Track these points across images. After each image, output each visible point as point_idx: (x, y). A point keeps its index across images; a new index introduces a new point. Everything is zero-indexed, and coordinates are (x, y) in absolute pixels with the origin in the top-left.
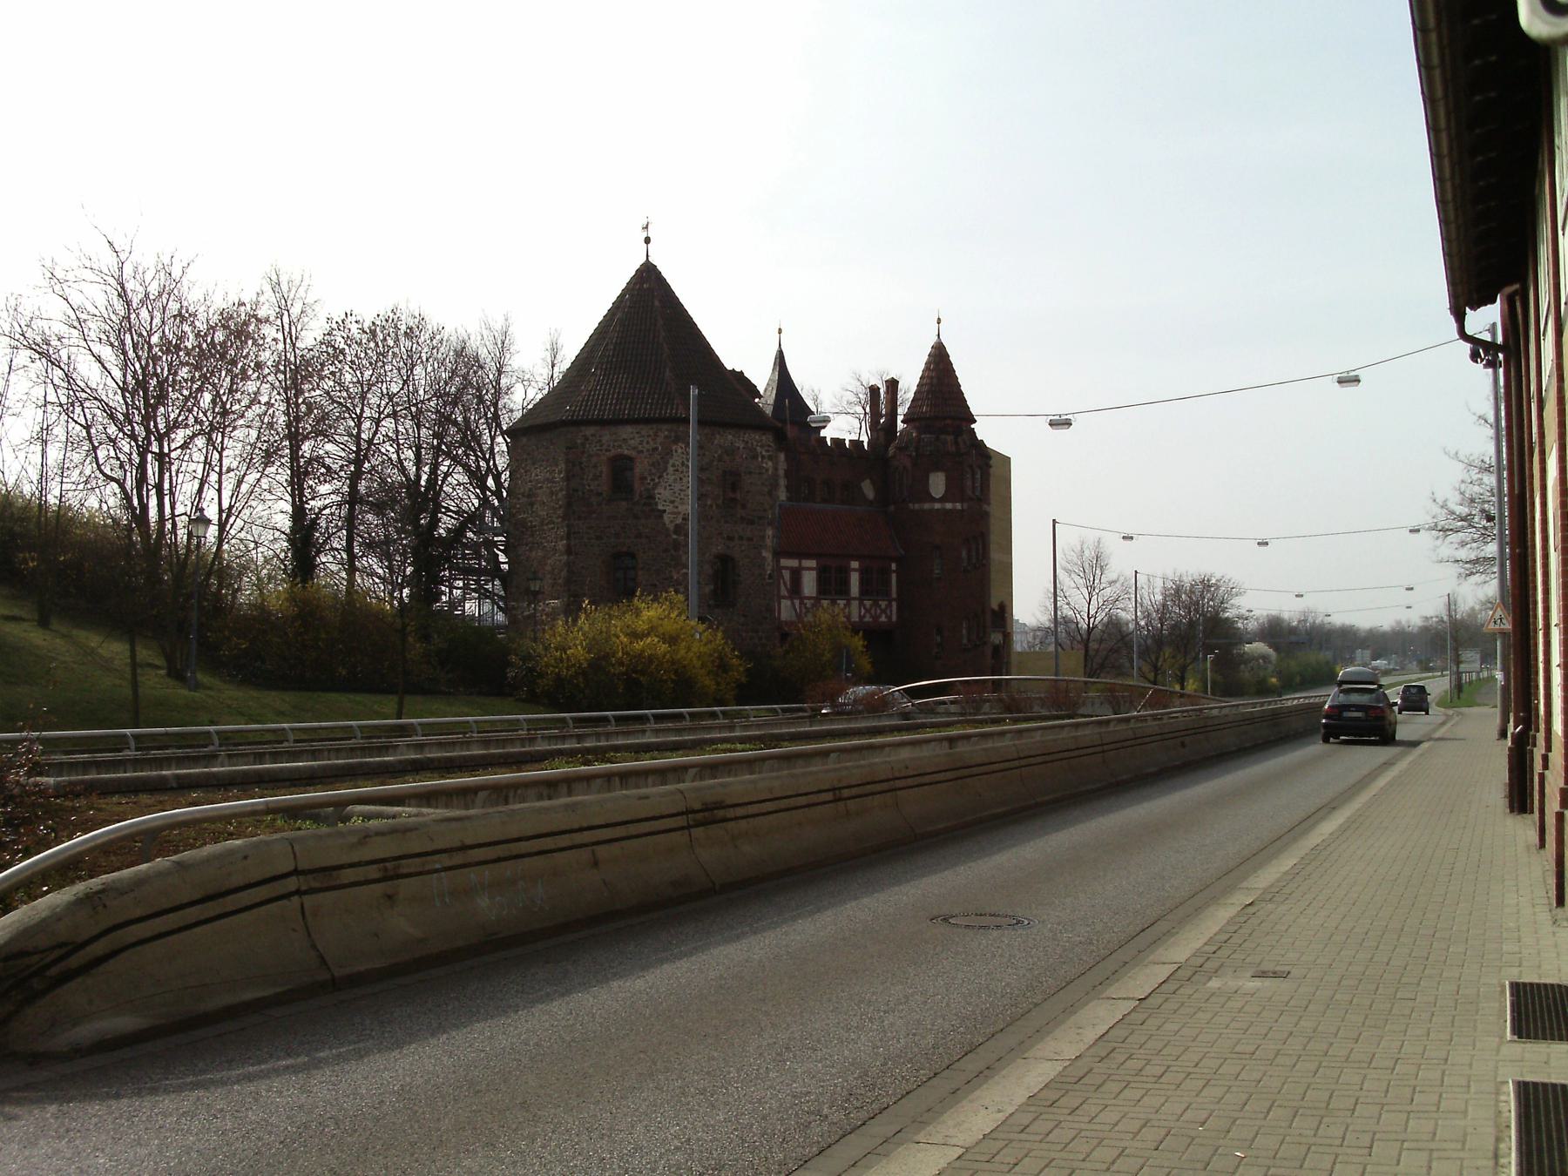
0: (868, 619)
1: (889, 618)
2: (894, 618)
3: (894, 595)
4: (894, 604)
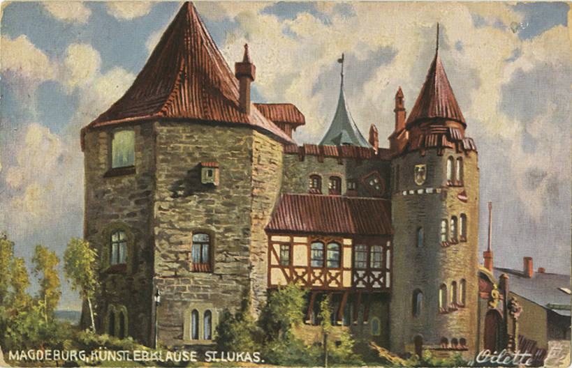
0: (360, 285)
1: (340, 284)
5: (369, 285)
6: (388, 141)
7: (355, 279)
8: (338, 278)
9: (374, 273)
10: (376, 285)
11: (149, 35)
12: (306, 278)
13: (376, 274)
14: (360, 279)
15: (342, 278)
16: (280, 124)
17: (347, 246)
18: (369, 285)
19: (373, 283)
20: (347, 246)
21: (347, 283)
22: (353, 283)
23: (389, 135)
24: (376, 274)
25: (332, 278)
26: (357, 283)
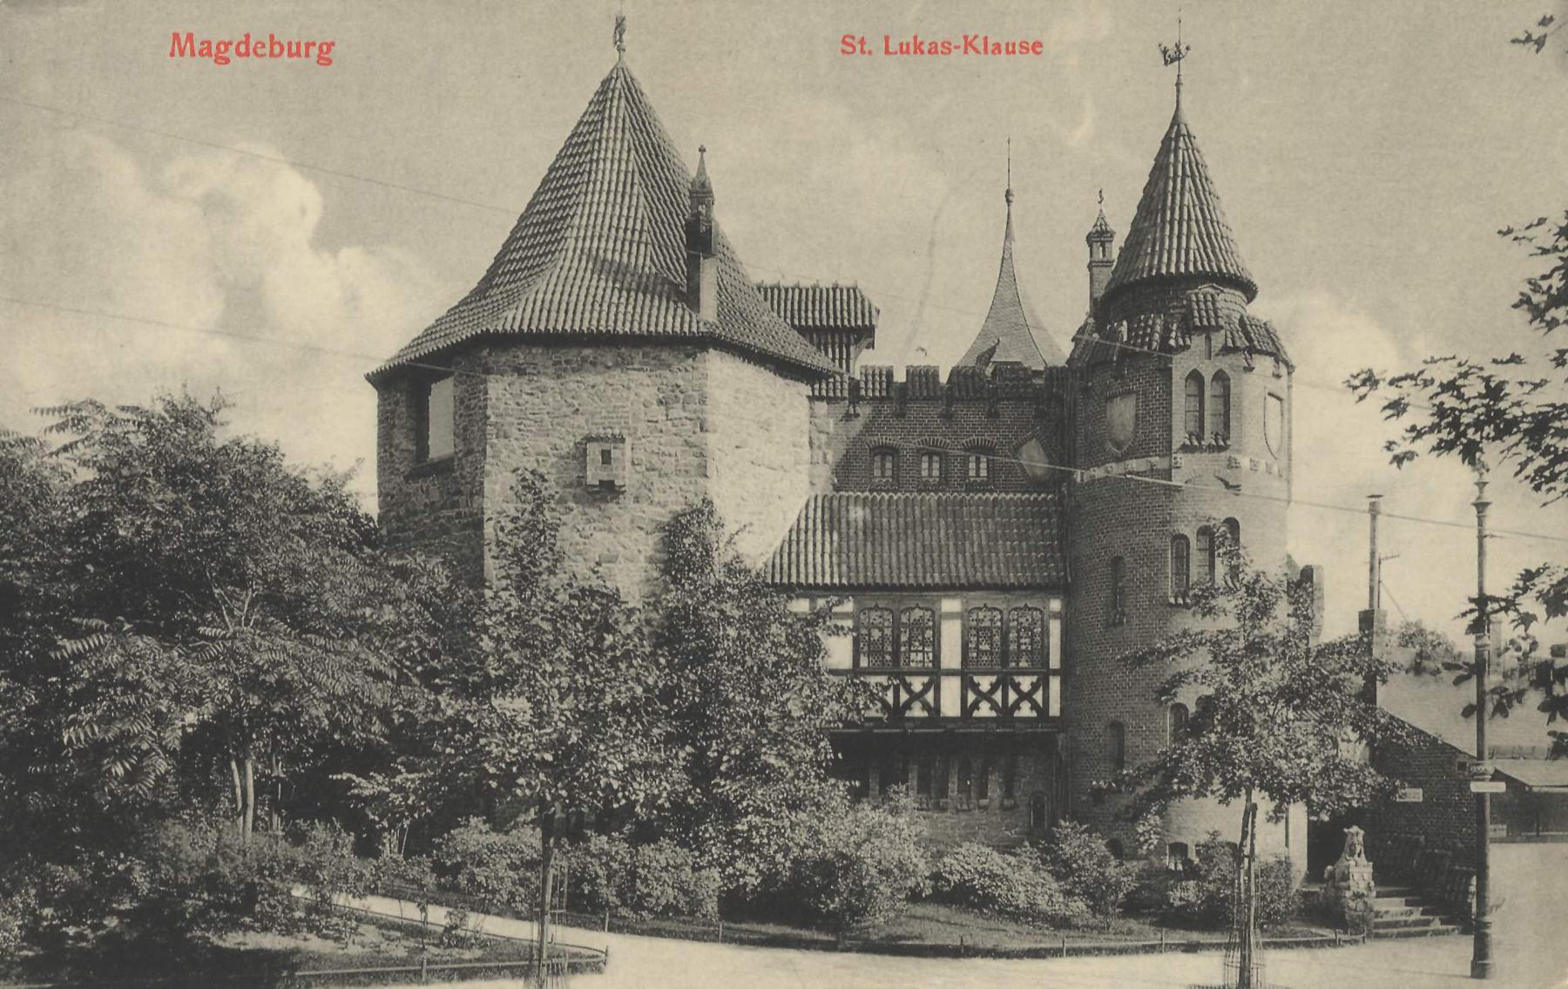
0: (985, 710)
1: (1042, 710)
2: (1055, 710)
3: (1055, 662)
4: (1055, 684)
5: (1006, 711)
6: (369, 400)
7: (971, 697)
8: (930, 697)
9: (1018, 679)
10: (1026, 711)
11: (296, 488)
12: (1012, 696)
13: (917, 684)
14: (1027, 697)
15: (937, 698)
16: (818, 334)
17: (951, 616)
18: (1006, 711)
19: (1017, 706)
20: (951, 616)
21: (951, 707)
22: (967, 710)
23: (387, 348)
24: (1026, 683)
25: (915, 697)
26: (975, 706)
